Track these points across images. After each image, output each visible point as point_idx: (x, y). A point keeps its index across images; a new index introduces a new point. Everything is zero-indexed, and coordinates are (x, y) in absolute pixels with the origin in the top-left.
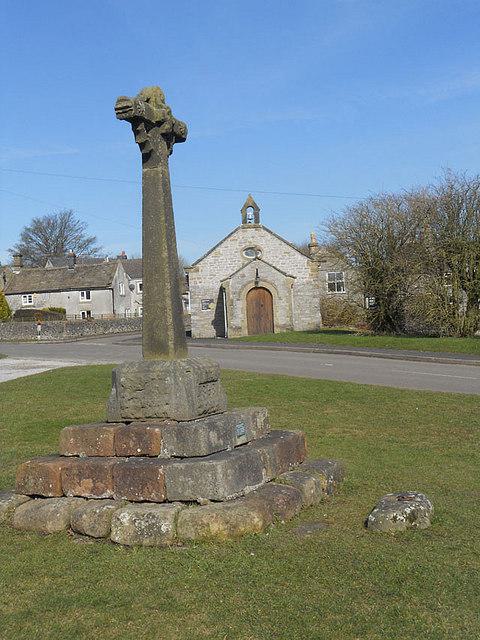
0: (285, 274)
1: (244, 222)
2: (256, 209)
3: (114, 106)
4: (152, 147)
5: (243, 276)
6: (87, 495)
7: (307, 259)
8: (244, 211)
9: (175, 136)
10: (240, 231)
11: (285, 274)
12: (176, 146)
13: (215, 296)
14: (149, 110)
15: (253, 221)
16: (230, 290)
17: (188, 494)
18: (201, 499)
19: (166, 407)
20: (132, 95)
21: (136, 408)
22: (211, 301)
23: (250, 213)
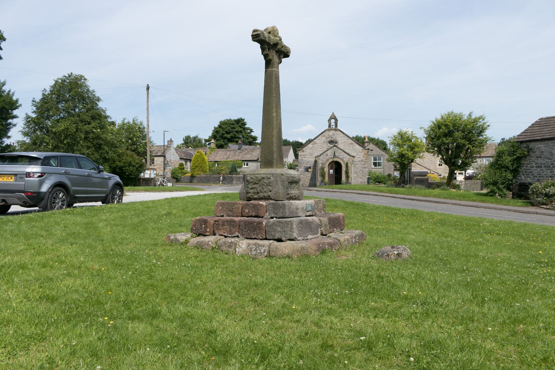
0: (349, 155)
1: (330, 126)
2: (336, 121)
3: (251, 33)
4: (271, 57)
5: (327, 155)
6: (226, 235)
7: (361, 148)
8: (329, 120)
9: (284, 53)
10: (327, 132)
11: (349, 155)
12: (284, 60)
13: (312, 165)
14: (269, 37)
15: (334, 127)
16: (320, 162)
17: (277, 236)
18: (284, 239)
19: (270, 193)
20: (261, 27)
21: (254, 193)
22: (310, 168)
23: (333, 121)
